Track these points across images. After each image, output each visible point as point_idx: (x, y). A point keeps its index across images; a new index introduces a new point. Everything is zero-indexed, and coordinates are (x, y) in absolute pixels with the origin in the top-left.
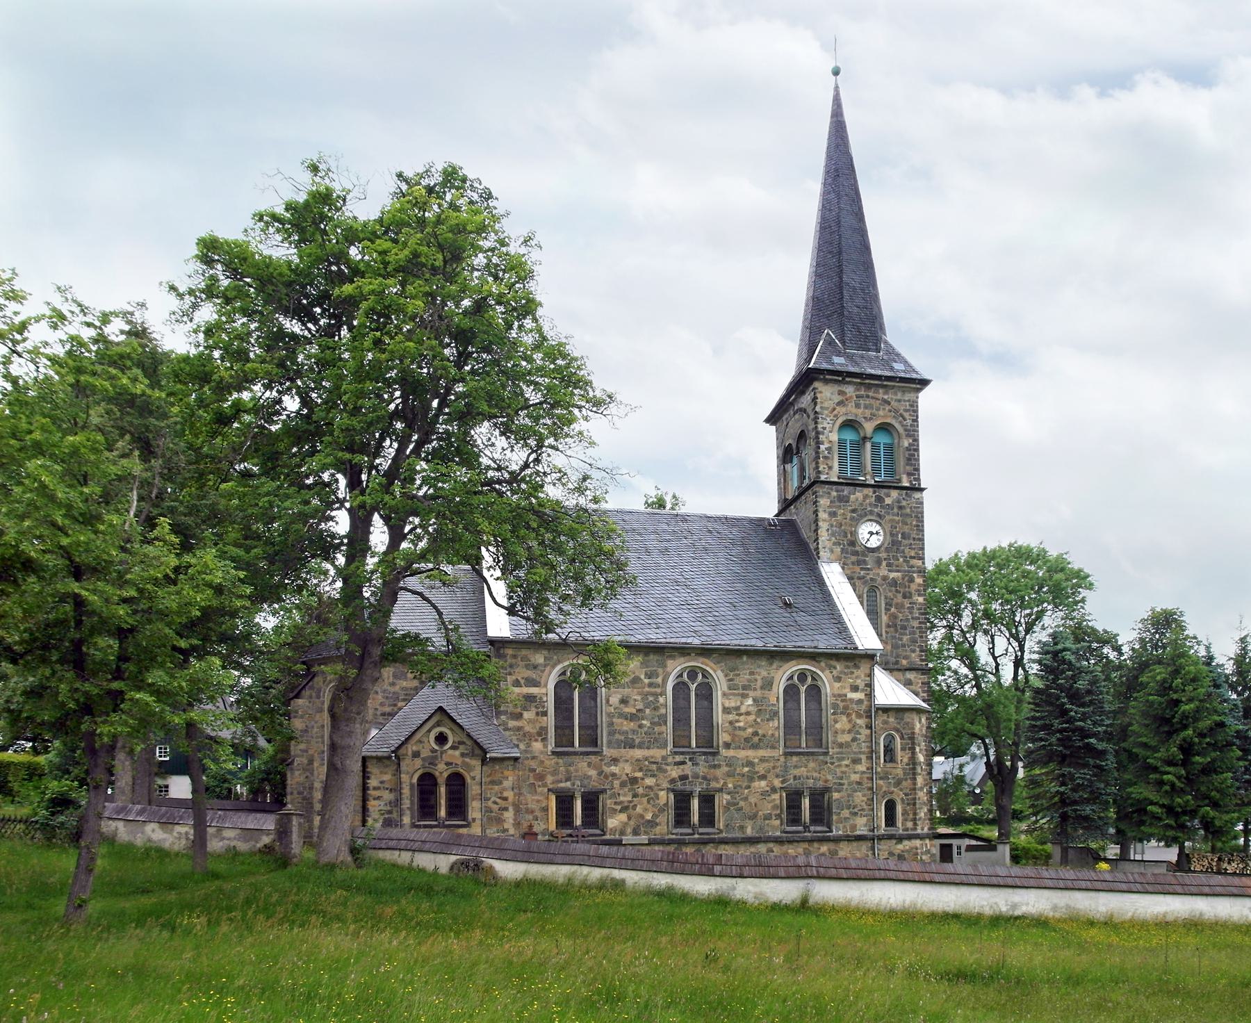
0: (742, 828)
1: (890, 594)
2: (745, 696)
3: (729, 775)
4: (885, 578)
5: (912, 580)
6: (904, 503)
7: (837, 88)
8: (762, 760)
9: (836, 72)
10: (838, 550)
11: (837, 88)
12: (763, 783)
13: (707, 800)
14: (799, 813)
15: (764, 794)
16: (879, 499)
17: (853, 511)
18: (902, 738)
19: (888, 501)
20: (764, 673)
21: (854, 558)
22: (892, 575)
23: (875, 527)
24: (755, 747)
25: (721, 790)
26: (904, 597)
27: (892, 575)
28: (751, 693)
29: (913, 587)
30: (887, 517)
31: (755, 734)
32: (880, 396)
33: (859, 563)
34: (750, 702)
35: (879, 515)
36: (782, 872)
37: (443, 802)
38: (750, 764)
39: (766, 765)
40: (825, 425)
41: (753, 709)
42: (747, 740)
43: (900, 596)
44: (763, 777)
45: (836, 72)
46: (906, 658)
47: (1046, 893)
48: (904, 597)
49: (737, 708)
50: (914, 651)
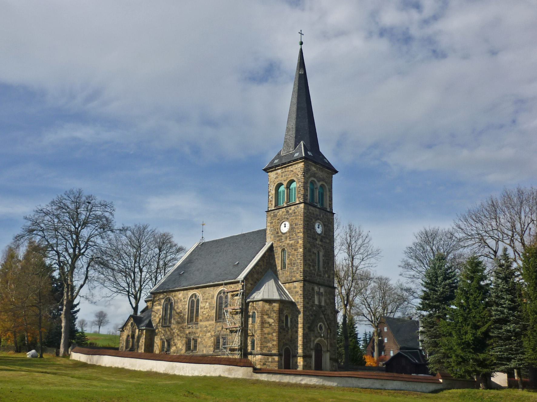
0: (203, 351)
1: (290, 251)
2: (206, 302)
3: (201, 331)
4: (288, 244)
5: (298, 243)
6: (296, 211)
7: (301, 49)
8: (210, 325)
9: (301, 43)
10: (273, 236)
11: (301, 49)
12: (209, 334)
13: (195, 341)
14: (219, 345)
15: (210, 338)
16: (287, 212)
17: (278, 219)
18: (258, 313)
19: (290, 212)
20: (212, 293)
21: (278, 239)
22: (291, 242)
23: (283, 225)
24: (208, 320)
25: (198, 337)
26: (295, 250)
27: (291, 242)
28: (208, 301)
29: (299, 245)
30: (290, 218)
31: (208, 316)
32: (290, 170)
33: (279, 240)
34: (208, 304)
35: (287, 219)
36: (242, 364)
37: (300, 325)
38: (206, 327)
39: (211, 327)
40: (271, 188)
41: (208, 307)
42: (206, 318)
43: (293, 250)
44: (209, 332)
45: (301, 43)
46: (295, 277)
47: (399, 382)
48: (295, 250)
49: (204, 307)
50: (297, 273)
